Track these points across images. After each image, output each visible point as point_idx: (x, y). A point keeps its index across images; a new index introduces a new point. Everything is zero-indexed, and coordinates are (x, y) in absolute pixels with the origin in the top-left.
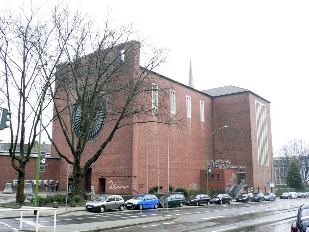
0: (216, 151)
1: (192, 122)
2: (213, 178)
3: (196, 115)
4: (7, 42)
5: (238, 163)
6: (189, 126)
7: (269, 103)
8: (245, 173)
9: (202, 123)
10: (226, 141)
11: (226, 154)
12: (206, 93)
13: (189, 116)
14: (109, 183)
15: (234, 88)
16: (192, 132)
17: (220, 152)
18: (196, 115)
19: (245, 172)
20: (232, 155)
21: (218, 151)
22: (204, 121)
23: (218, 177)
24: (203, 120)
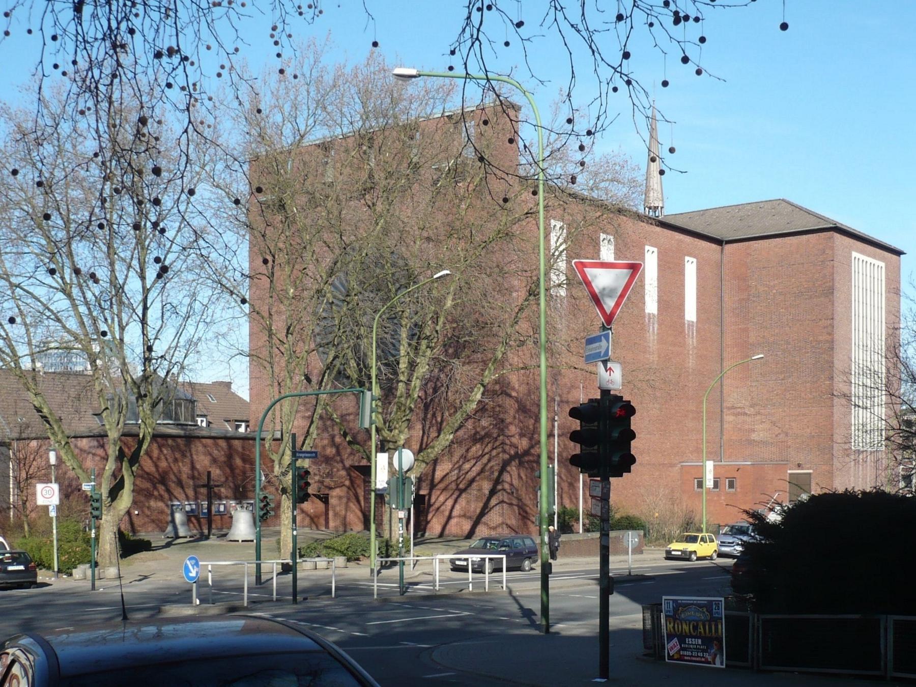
0: (729, 408)
1: (660, 325)
2: (733, 490)
3: (671, 300)
4: (188, 109)
5: (789, 443)
6: (692, 341)
7: (899, 253)
8: (810, 474)
9: (689, 325)
10: (759, 379)
11: (758, 417)
12: (672, 222)
13: (651, 306)
14: (856, 616)
15: (790, 208)
16: (659, 357)
17: (739, 410)
18: (671, 300)
19: (811, 471)
20: (774, 419)
21: (733, 408)
22: (655, 312)
23: (731, 485)
24: (691, 313)
